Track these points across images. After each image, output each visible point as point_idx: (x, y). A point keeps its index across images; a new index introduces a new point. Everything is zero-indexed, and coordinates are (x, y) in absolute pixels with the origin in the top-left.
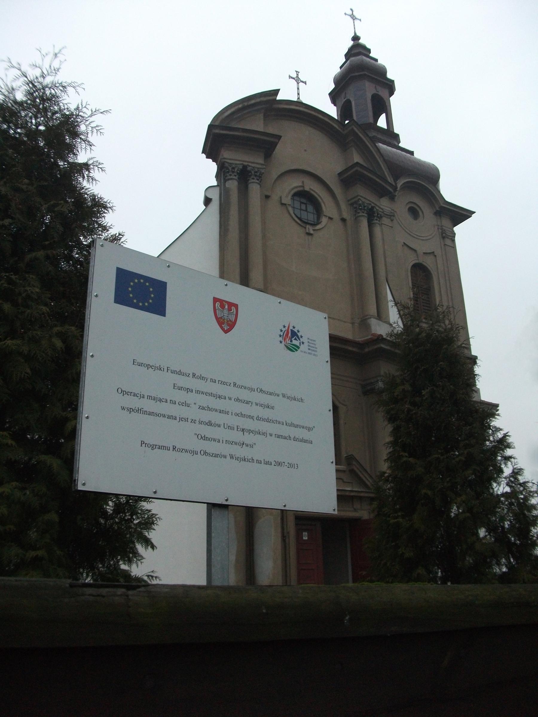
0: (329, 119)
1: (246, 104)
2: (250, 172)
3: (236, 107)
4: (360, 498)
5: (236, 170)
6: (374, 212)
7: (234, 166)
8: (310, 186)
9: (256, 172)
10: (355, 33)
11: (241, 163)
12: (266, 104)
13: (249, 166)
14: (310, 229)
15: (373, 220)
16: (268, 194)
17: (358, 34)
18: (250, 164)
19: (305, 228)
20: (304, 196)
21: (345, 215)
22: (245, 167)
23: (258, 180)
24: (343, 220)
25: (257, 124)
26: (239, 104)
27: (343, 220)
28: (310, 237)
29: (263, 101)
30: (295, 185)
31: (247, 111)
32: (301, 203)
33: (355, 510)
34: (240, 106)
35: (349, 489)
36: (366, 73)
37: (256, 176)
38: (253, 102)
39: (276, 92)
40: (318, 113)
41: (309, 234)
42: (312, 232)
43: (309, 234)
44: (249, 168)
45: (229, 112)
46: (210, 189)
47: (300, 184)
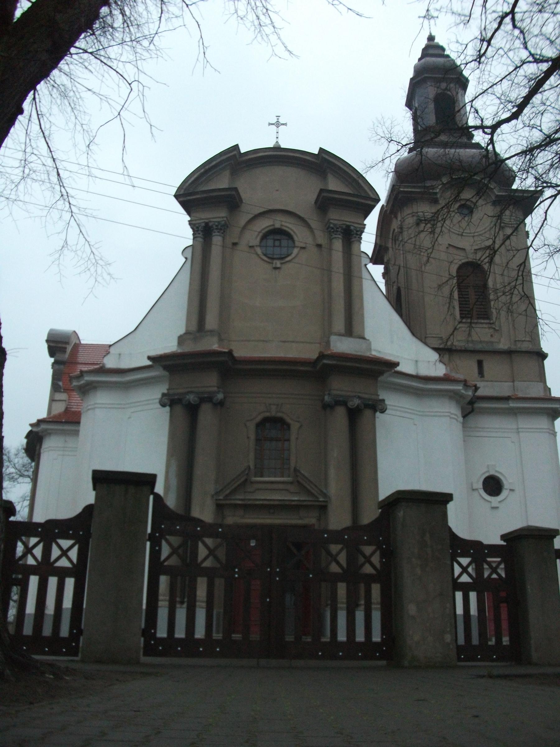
0: (300, 154)
1: (207, 167)
2: (212, 227)
3: (199, 173)
4: (307, 507)
5: (200, 228)
6: (351, 231)
7: (197, 225)
8: (279, 222)
9: (216, 226)
10: (430, 33)
11: (203, 221)
12: (232, 161)
13: (211, 222)
14: (278, 263)
15: (351, 239)
16: (235, 241)
17: (433, 34)
18: (212, 220)
19: (272, 263)
20: (278, 234)
21: (320, 241)
22: (207, 224)
23: (218, 232)
24: (319, 246)
25: (222, 182)
26: (202, 169)
27: (319, 246)
28: (277, 271)
29: (223, 160)
30: (267, 224)
31: (210, 173)
32: (275, 240)
33: (301, 518)
34: (202, 170)
35: (296, 499)
36: (426, 75)
37: (216, 229)
38: (214, 163)
39: (236, 147)
40: (294, 153)
41: (276, 268)
42: (278, 265)
43: (276, 268)
44: (210, 224)
45: (193, 179)
46: (186, 250)
47: (272, 223)
